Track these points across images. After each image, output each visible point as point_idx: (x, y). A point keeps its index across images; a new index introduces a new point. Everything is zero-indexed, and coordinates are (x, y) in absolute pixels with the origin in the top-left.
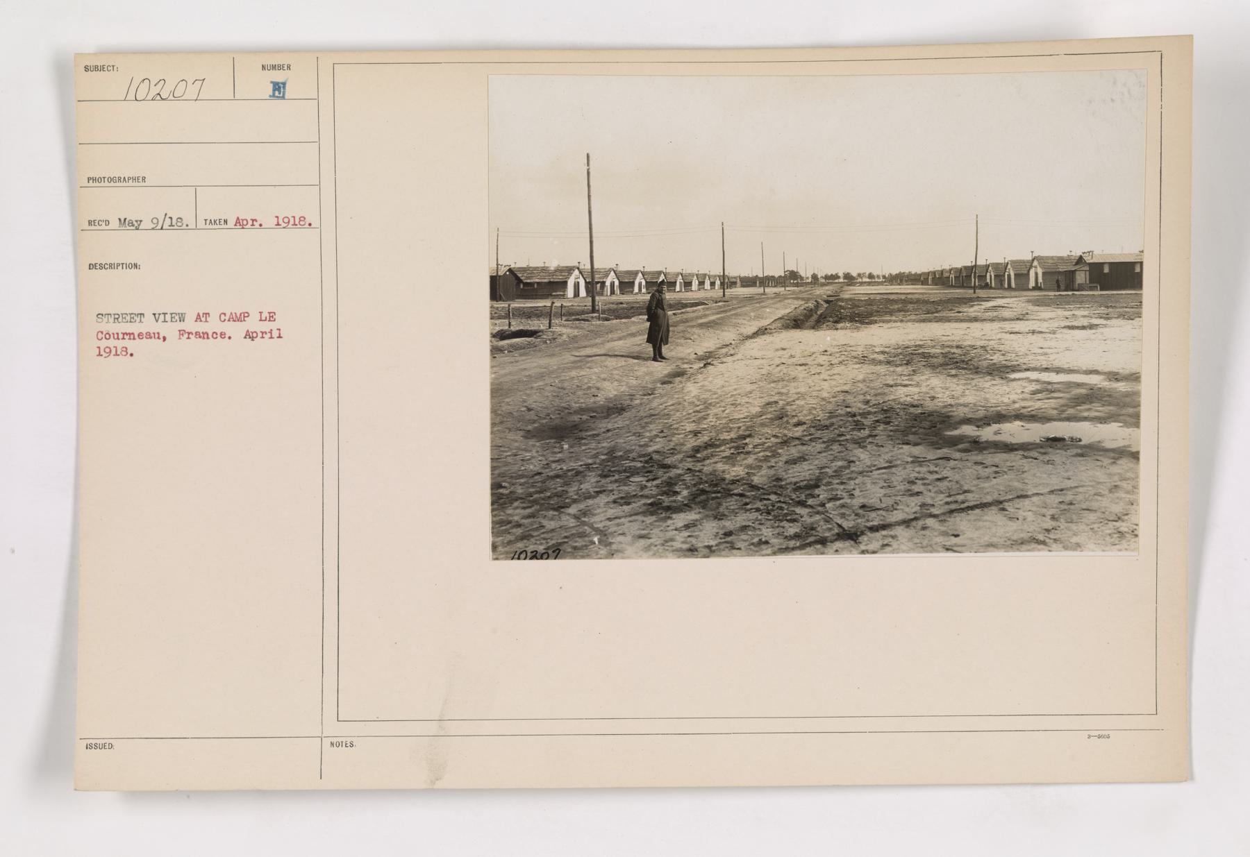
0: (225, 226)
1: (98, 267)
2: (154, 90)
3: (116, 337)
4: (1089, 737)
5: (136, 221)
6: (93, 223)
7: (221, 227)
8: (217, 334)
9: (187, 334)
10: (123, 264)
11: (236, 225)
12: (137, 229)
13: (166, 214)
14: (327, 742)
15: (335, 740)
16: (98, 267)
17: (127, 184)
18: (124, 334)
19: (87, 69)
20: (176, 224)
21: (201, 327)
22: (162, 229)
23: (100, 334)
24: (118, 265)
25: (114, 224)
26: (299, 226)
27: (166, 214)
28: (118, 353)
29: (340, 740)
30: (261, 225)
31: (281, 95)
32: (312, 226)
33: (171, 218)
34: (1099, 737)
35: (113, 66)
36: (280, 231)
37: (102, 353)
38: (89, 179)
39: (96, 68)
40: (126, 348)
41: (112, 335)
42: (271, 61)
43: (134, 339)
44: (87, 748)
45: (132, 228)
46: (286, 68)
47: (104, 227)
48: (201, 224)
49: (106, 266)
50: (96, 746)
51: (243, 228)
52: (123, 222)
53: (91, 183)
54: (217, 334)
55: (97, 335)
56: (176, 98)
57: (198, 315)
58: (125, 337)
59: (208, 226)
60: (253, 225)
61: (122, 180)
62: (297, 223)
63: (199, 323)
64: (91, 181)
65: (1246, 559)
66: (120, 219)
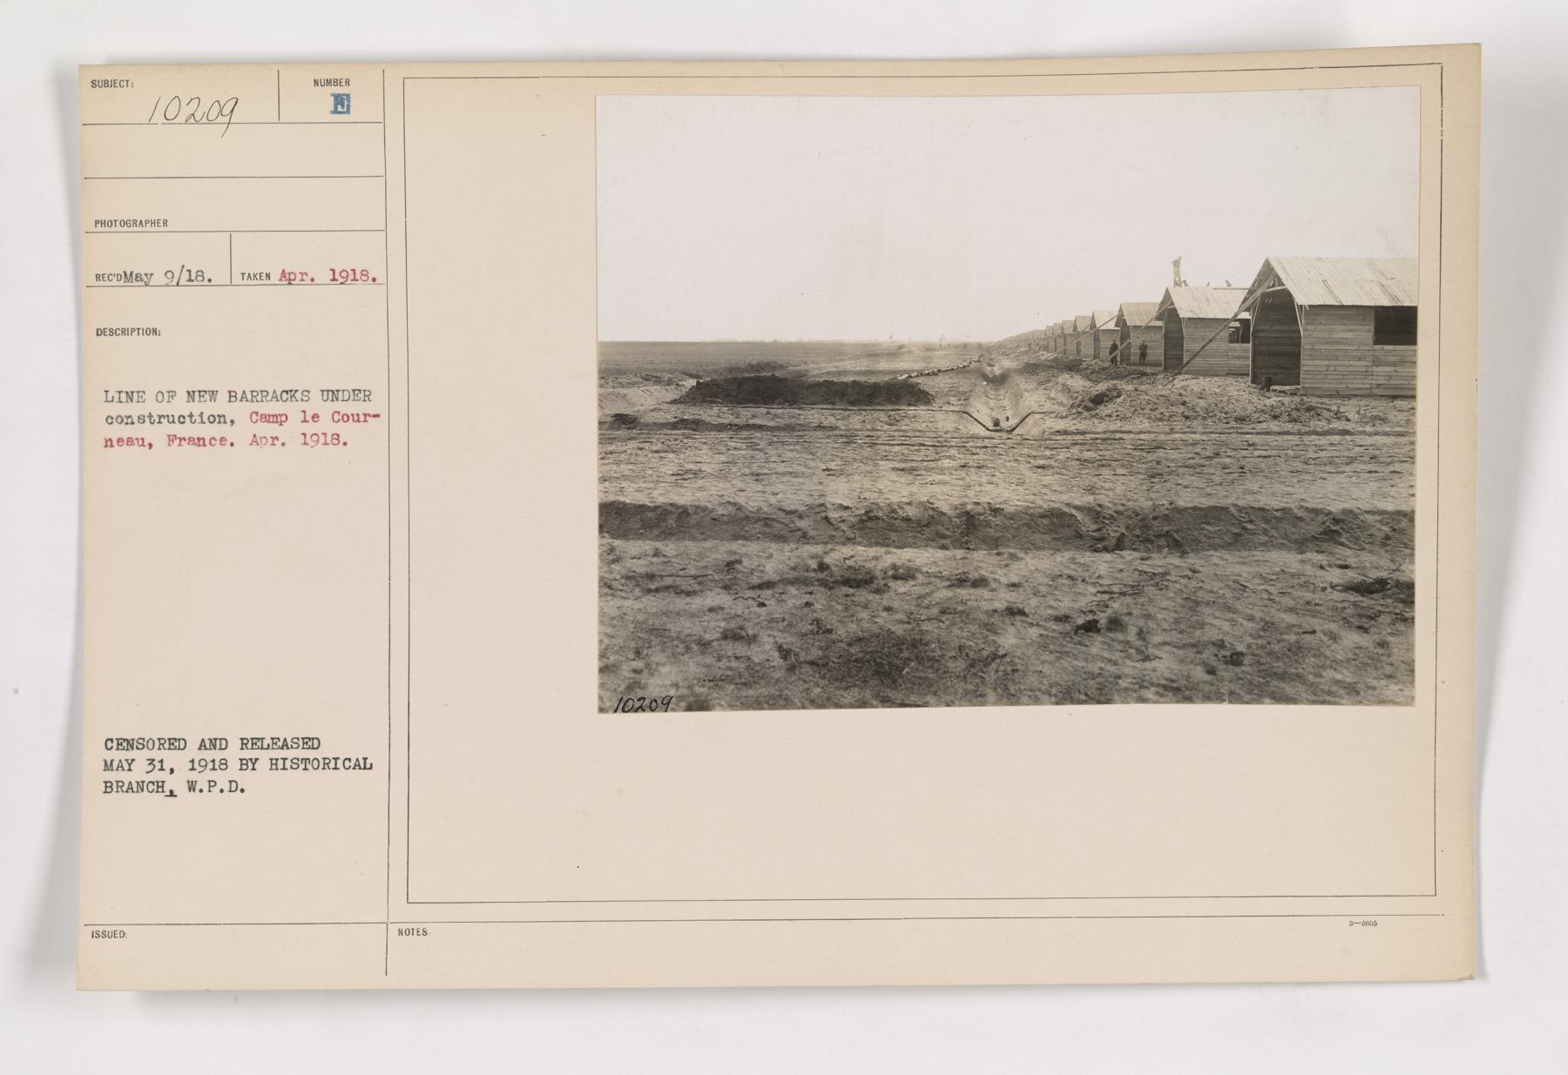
0: (268, 282)
1: (108, 333)
2: (186, 111)
3: (356, 418)
4: (1352, 924)
5: (146, 275)
7: (261, 282)
8: (112, 418)
9: (178, 440)
10: (138, 329)
11: (280, 280)
12: (147, 285)
14: (394, 929)
15: (403, 927)
16: (108, 333)
17: (144, 229)
18: (160, 417)
19: (94, 84)
20: (196, 278)
21: (165, 409)
22: (177, 285)
23: (254, 415)
24: (133, 330)
29: (410, 926)
30: (312, 280)
31: (345, 110)
32: (377, 282)
33: (189, 271)
34: (1365, 924)
35: (127, 81)
36: (336, 288)
38: (97, 222)
39: (106, 83)
40: (338, 435)
41: (351, 418)
42: (323, 75)
46: (343, 83)
48: (237, 279)
49: (118, 332)
50: (104, 935)
51: (290, 284)
54: (184, 418)
55: (333, 416)
56: (210, 122)
59: (245, 282)
60: (302, 280)
61: (138, 223)
65: (1563, 702)
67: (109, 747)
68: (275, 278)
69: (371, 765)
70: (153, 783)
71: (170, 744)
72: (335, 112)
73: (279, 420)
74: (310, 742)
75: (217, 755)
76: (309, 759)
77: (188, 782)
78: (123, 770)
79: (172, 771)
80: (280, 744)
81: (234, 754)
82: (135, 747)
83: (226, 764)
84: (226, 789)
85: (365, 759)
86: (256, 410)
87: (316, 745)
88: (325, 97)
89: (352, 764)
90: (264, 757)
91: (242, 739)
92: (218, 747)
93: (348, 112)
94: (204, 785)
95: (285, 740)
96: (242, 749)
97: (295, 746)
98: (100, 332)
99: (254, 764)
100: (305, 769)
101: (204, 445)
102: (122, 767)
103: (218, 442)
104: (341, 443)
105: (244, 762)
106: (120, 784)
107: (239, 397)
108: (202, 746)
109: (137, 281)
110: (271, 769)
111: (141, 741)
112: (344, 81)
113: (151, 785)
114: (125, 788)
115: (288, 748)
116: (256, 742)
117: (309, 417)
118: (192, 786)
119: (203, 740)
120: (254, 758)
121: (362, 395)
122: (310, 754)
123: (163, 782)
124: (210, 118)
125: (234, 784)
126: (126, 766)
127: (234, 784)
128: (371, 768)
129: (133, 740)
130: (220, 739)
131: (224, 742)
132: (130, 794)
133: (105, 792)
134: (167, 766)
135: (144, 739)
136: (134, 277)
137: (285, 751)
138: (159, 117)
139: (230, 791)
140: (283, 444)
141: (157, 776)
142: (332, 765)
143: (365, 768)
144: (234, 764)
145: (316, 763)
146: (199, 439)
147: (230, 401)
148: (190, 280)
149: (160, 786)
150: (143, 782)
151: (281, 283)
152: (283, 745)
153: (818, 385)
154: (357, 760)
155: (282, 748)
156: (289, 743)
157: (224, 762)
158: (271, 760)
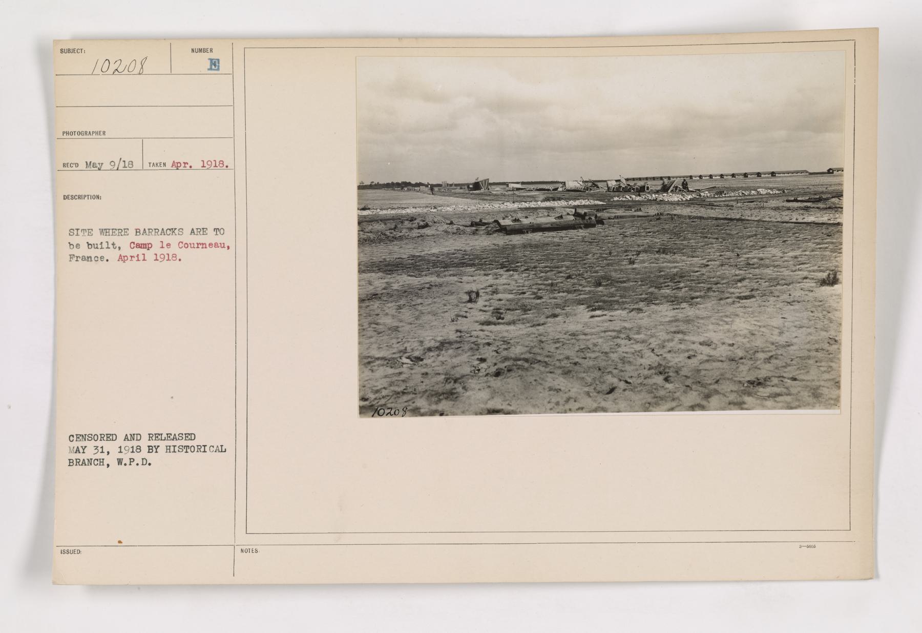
0: (164, 168)
1: (70, 198)
2: (113, 67)
5: (99, 164)
6: (66, 165)
7: (160, 168)
10: (88, 196)
11: (172, 167)
12: (99, 169)
13: (121, 159)
14: (238, 549)
15: (244, 548)
16: (70, 198)
17: (92, 137)
18: (198, 244)
19: (62, 51)
20: (129, 165)
22: (117, 170)
23: (132, 244)
25: (82, 166)
26: (219, 168)
27: (121, 159)
28: (170, 258)
29: (248, 547)
30: (191, 167)
31: (217, 68)
32: (228, 168)
33: (124, 161)
34: (808, 547)
35: (81, 49)
37: (158, 258)
39: (69, 51)
43: (206, 247)
44: (61, 553)
45: (95, 169)
46: (209, 51)
47: (74, 168)
48: (146, 166)
49: (76, 197)
50: (68, 552)
51: (178, 169)
52: (88, 164)
53: (65, 136)
57: (193, 229)
58: (199, 246)
59: (151, 168)
61: (88, 133)
62: (217, 165)
63: (193, 235)
64: (65, 134)
65: (919, 413)
66: (86, 162)
67: (71, 440)
68: (169, 165)
69: (225, 449)
70: (97, 460)
71: (107, 437)
72: (211, 69)
73: (147, 247)
74: (190, 436)
75: (135, 443)
76: (189, 446)
77: (118, 459)
78: (80, 453)
79: (108, 453)
80: (172, 437)
81: (144, 443)
82: (87, 439)
83: (140, 449)
84: (140, 463)
85: (222, 446)
86: (182, 241)
87: (193, 438)
88: (203, 60)
89: (215, 449)
90: (163, 445)
91: (149, 434)
92: (135, 439)
93: (218, 69)
94: (127, 461)
95: (175, 435)
96: (149, 440)
97: (181, 438)
98: (66, 197)
99: (156, 449)
100: (187, 452)
101: (91, 261)
102: (79, 451)
103: (99, 259)
104: (178, 259)
105: (151, 448)
106: (78, 461)
107: (142, 232)
108: (126, 438)
109: (94, 167)
110: (167, 452)
111: (90, 436)
112: (209, 50)
113: (96, 461)
114: (81, 463)
115: (176, 440)
116: (158, 436)
117: (165, 245)
118: (120, 461)
119: (126, 435)
120: (157, 445)
121: (117, 232)
122: (189, 443)
123: (103, 459)
124: (130, 70)
125: (145, 461)
126: (81, 450)
127: (145, 461)
128: (225, 451)
129: (85, 435)
130: (137, 434)
131: (139, 436)
132: (84, 466)
133: (69, 465)
134: (105, 450)
135: (92, 435)
136: (92, 165)
137: (175, 441)
138: (98, 71)
139: (143, 465)
140: (107, 260)
141: (100, 456)
142: (202, 449)
143: (222, 451)
144: (145, 449)
145: (192, 449)
146: (88, 258)
147: (136, 235)
148: (125, 167)
149: (101, 462)
150: (91, 459)
151: (172, 168)
152: (174, 438)
153: (537, 228)
154: (218, 446)
155: (173, 440)
156: (177, 437)
157: (139, 447)
158: (167, 446)
